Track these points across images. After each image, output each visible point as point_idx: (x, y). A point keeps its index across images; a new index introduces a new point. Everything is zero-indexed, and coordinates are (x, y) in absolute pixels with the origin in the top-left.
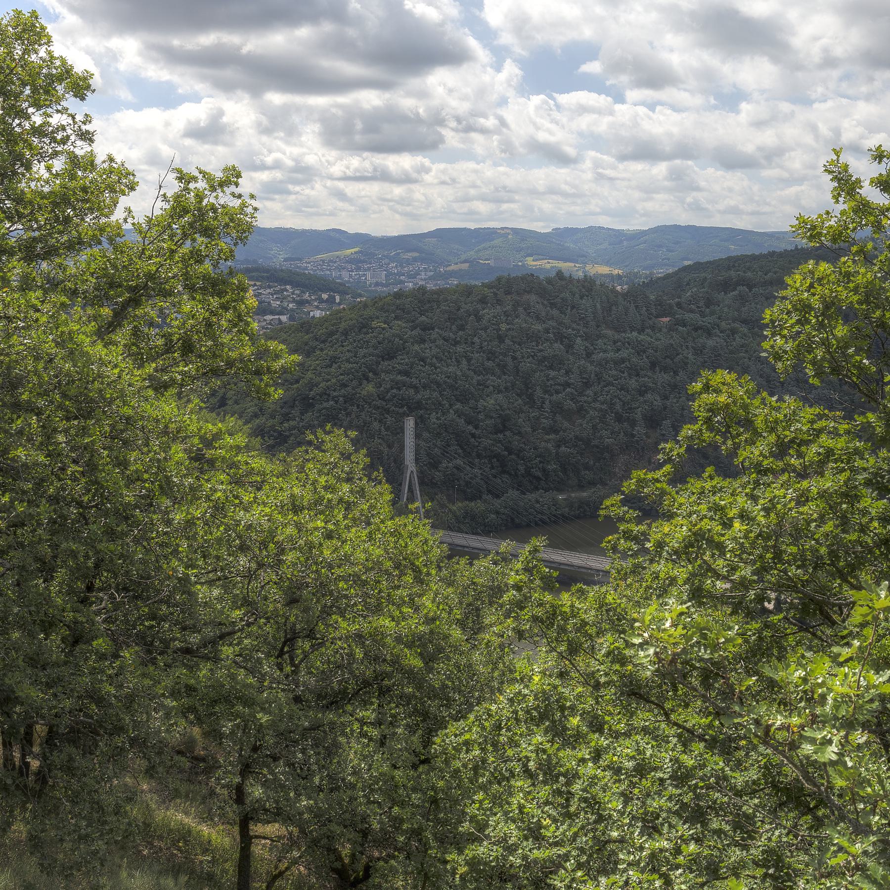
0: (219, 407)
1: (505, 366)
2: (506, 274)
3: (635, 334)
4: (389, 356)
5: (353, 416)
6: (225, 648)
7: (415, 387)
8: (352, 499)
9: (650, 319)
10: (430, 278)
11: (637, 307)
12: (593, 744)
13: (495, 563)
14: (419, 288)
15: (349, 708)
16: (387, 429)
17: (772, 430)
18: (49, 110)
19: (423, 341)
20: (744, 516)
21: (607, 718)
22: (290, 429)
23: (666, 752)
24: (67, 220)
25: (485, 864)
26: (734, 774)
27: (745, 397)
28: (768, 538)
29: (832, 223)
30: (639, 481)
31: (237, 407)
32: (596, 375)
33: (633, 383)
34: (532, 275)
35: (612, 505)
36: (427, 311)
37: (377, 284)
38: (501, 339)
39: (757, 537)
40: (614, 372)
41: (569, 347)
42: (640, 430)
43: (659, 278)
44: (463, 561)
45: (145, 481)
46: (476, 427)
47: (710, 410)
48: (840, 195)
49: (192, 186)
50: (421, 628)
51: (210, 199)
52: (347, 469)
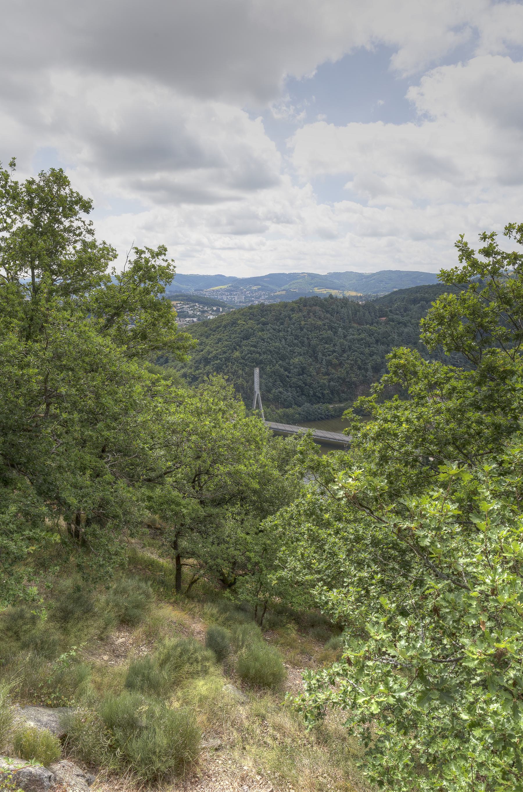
0: (165, 364)
1: (303, 343)
2: (304, 297)
3: (368, 326)
4: (246, 338)
5: (229, 367)
6: (168, 479)
7: (259, 353)
8: (226, 409)
9: (376, 318)
10: (266, 299)
11: (369, 312)
12: (335, 527)
13: (296, 439)
14: (261, 304)
15: (226, 507)
16: (246, 374)
17: (426, 377)
18: (72, 219)
19: (263, 330)
20: (408, 421)
21: (344, 514)
22: (199, 374)
23: (369, 532)
24: (84, 274)
25: (286, 580)
26: (401, 543)
27: (414, 360)
28: (418, 432)
29: (459, 273)
30: (362, 402)
31: (173, 363)
32: (349, 347)
33: (367, 350)
34: (317, 297)
35: (348, 413)
36: (265, 315)
37: (240, 302)
38: (301, 329)
39: (414, 431)
40: (358, 345)
41: (335, 333)
42: (370, 373)
43: (381, 298)
44: (280, 438)
45: (124, 402)
46: (289, 373)
47: (396, 367)
48: (462, 258)
49: (143, 256)
50: (259, 470)
51: (152, 262)
52: (224, 394)
